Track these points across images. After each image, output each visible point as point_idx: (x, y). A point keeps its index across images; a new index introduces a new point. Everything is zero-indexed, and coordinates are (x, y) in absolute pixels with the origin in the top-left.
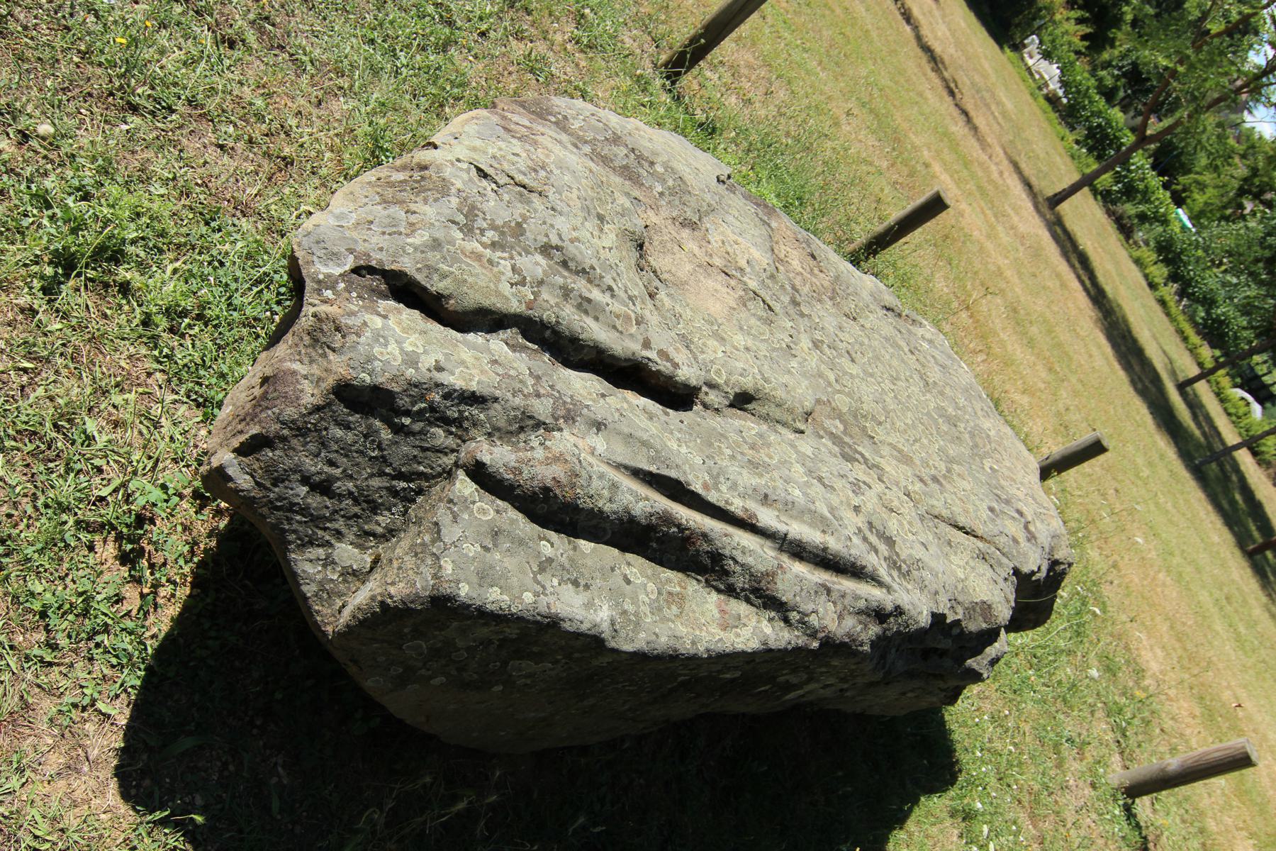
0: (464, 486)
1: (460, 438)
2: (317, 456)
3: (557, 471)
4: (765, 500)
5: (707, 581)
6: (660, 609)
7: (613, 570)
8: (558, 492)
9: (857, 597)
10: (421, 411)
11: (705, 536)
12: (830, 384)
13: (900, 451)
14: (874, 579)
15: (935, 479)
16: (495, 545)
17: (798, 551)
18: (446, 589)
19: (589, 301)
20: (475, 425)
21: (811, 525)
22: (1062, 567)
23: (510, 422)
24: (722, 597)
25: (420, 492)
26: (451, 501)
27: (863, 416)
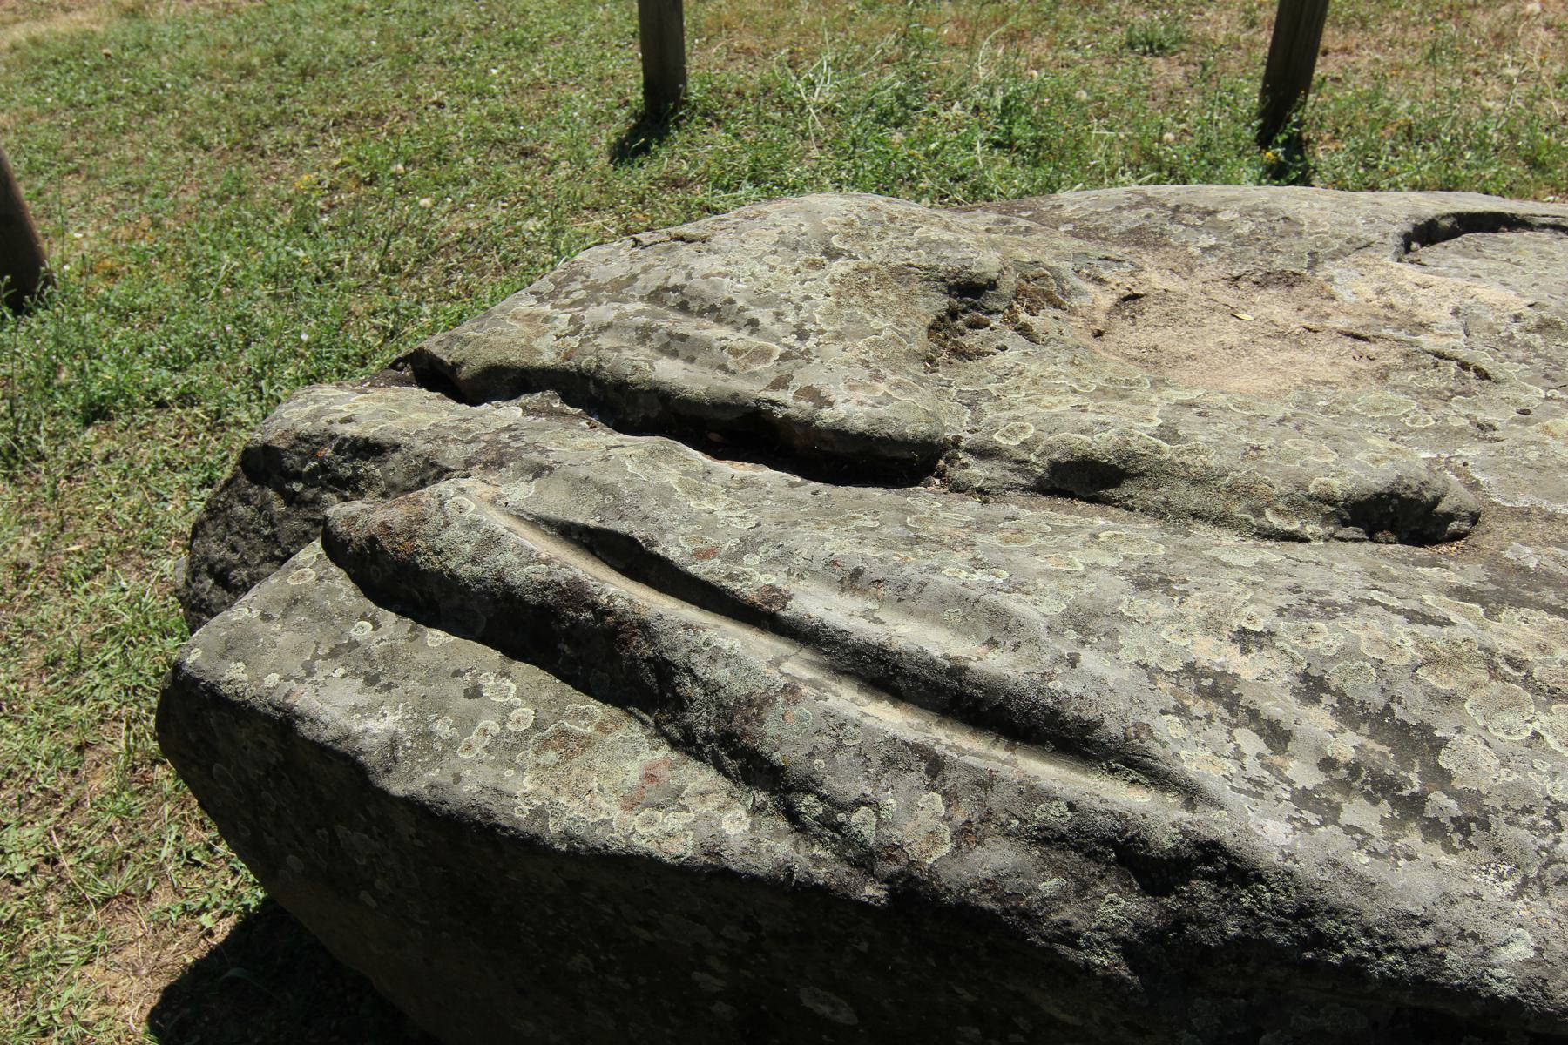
2: (222, 541)
5: (657, 724)
8: (384, 543)
9: (1034, 794)
10: (313, 471)
11: (644, 626)
17: (882, 673)
19: (683, 338)
23: (408, 475)
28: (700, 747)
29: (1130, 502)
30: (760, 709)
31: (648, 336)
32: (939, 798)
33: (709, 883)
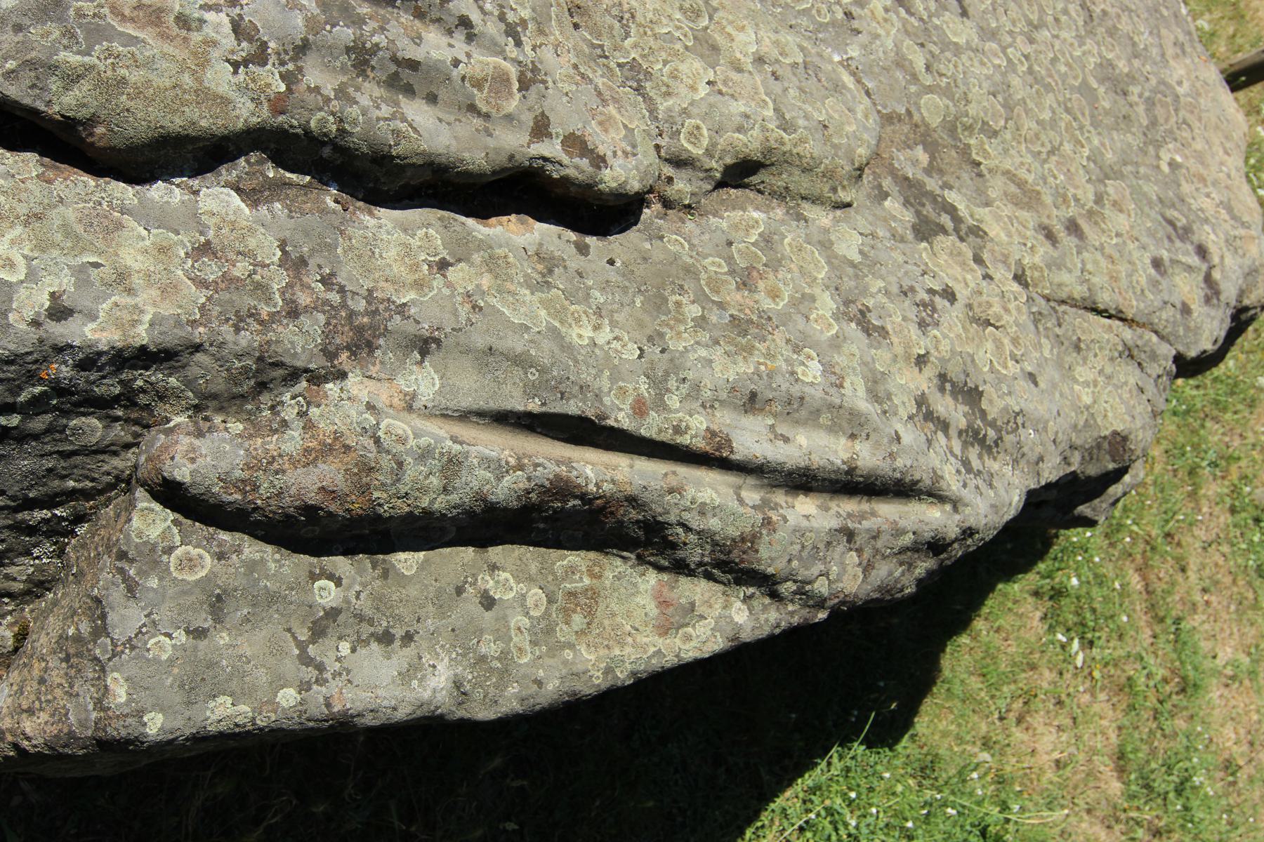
0: (151, 522)
1: (136, 422)
3: (331, 473)
4: (752, 403)
5: (639, 557)
6: (550, 631)
7: (459, 591)
9: (899, 532)
12: (914, 78)
13: (1021, 184)
14: (935, 495)
15: (1073, 227)
16: (218, 620)
17: (803, 481)
18: (117, 730)
19: (413, 65)
20: (162, 397)
21: (833, 429)
22: (1252, 312)
23: (233, 380)
24: (665, 577)
25: (79, 519)
26: (122, 556)
27: (969, 128)
28: (693, 570)
29: (761, 187)
30: (752, 543)
31: (366, 62)
32: (854, 554)
33: (740, 659)
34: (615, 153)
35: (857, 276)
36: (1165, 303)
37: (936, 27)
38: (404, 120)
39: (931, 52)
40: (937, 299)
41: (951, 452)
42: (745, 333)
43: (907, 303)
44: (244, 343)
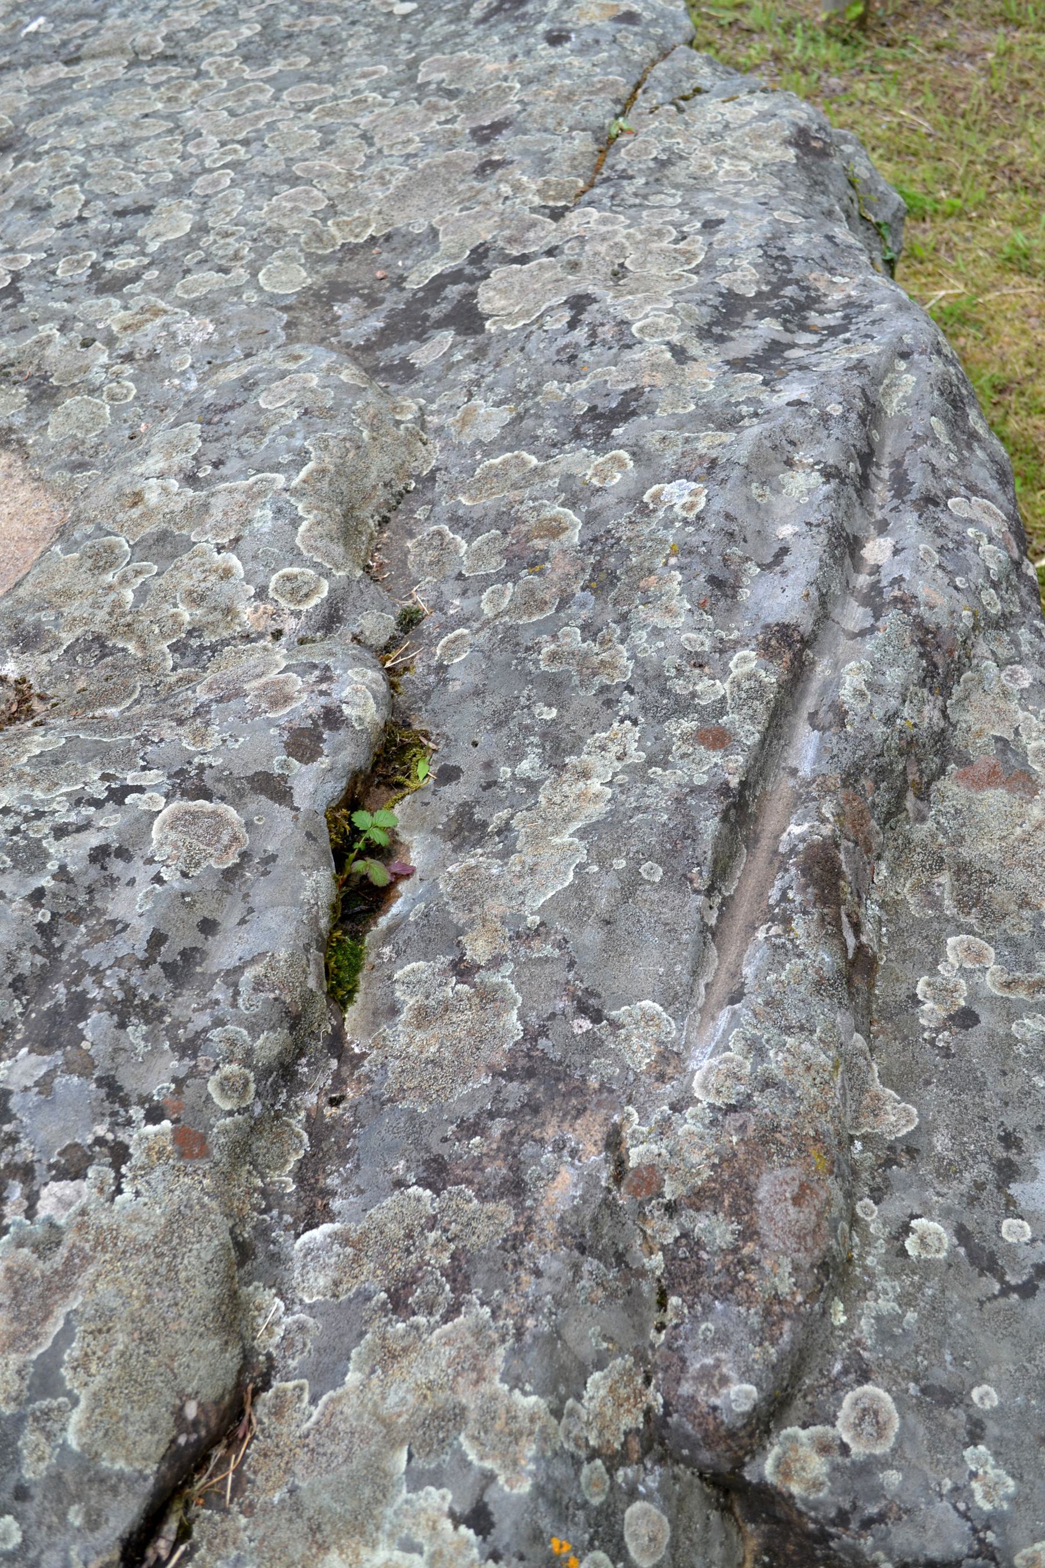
15: (484, 135)
19: (157, 939)
32: (950, 502)
34: (322, 693)
35: (538, 416)
36: (615, 41)
37: (164, 248)
38: (238, 970)
39: (199, 262)
40: (585, 317)
41: (815, 346)
42: (613, 578)
43: (586, 356)
44: (555, 1266)
